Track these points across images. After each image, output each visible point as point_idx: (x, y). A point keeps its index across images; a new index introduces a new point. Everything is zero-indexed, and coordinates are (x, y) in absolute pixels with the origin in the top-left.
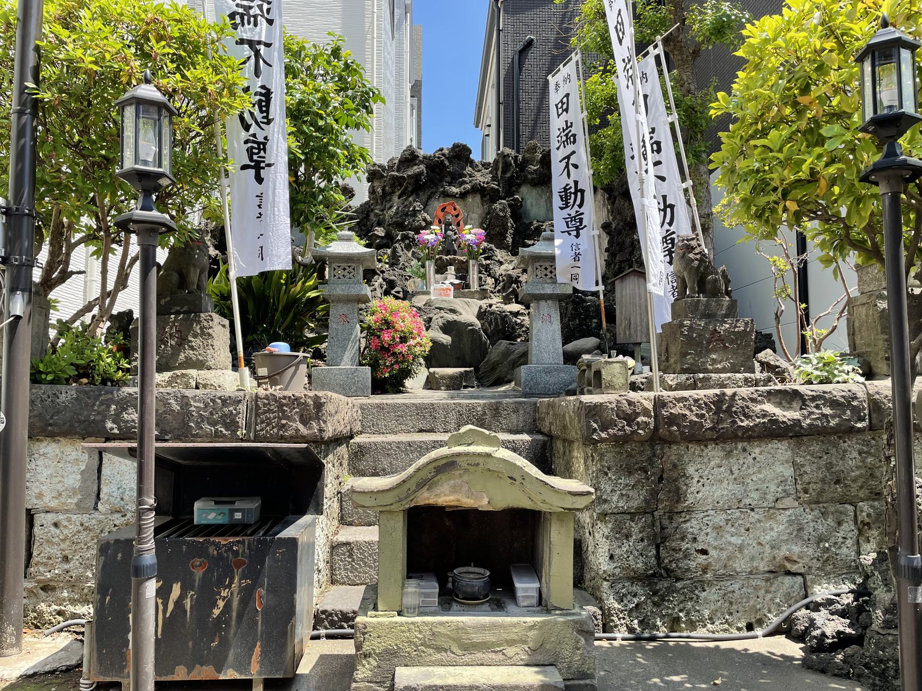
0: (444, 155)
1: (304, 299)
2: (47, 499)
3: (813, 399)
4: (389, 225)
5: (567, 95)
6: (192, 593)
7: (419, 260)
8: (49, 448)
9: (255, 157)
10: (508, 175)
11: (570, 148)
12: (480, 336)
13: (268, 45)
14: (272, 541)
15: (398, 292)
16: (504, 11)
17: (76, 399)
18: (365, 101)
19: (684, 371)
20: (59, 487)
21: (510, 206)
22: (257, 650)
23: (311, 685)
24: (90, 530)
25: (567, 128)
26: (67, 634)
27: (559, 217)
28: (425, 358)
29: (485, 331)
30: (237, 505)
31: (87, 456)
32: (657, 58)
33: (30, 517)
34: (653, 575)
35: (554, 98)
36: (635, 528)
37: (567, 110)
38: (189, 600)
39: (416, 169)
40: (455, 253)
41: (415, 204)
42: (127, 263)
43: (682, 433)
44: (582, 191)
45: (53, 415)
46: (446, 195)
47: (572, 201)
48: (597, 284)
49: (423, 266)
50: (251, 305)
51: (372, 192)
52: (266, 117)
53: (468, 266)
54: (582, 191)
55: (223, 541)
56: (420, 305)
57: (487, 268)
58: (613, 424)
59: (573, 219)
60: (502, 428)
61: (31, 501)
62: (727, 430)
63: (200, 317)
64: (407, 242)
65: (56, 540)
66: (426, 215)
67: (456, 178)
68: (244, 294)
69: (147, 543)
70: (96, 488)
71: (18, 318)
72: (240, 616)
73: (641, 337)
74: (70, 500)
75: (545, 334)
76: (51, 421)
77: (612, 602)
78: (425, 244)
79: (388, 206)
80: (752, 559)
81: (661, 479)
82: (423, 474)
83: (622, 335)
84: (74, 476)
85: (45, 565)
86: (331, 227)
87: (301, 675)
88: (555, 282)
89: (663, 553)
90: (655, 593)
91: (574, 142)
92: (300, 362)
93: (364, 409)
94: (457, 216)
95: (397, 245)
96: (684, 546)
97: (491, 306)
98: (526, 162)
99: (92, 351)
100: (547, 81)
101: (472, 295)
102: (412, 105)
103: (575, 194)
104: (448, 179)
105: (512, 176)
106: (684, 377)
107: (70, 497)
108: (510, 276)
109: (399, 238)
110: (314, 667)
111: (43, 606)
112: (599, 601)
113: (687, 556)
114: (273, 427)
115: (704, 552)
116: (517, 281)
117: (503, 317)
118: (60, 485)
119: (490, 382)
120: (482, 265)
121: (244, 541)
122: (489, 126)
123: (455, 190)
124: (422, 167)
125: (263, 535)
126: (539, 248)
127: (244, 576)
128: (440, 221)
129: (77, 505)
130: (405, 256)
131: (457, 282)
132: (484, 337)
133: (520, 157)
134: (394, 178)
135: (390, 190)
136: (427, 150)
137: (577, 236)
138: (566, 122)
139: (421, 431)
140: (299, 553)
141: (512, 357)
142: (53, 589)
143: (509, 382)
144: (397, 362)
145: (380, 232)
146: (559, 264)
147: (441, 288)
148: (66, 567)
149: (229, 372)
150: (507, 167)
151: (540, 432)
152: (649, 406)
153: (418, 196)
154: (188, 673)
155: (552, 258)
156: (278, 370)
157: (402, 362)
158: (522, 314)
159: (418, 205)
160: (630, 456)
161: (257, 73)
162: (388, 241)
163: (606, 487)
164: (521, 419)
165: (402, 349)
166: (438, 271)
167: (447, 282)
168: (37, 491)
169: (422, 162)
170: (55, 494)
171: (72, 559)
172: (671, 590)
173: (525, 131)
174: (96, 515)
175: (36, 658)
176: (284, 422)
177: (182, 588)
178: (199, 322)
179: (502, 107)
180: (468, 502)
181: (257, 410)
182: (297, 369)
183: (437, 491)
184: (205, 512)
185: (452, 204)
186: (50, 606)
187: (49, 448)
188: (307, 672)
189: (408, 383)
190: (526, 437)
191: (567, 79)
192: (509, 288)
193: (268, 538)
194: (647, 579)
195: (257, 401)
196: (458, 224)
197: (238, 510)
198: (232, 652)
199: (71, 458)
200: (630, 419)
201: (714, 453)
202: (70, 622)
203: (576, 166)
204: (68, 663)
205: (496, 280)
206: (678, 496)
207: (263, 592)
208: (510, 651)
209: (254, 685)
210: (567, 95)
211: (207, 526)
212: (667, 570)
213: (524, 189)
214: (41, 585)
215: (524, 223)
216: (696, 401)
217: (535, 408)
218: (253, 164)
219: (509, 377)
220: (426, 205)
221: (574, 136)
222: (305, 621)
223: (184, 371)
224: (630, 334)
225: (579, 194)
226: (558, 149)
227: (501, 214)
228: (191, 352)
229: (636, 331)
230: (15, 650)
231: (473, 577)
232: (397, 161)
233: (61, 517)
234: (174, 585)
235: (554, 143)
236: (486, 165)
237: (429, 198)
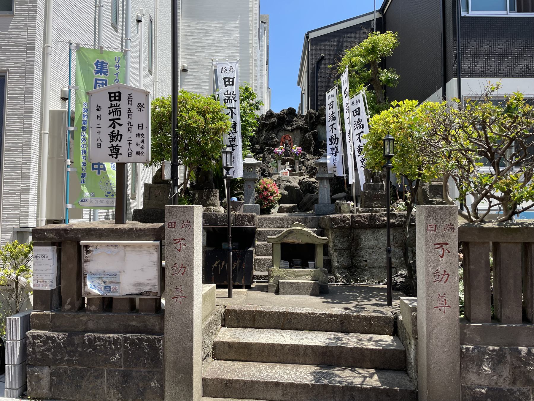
0: (284, 113)
3: (399, 216)
5: (333, 102)
10: (312, 121)
11: (333, 122)
12: (300, 192)
13: (235, 108)
19: (365, 207)
22: (244, 278)
28: (278, 201)
32: (363, 95)
34: (350, 267)
35: (328, 102)
36: (345, 254)
37: (332, 107)
43: (359, 226)
44: (338, 138)
48: (343, 174)
49: (276, 162)
52: (235, 131)
56: (275, 179)
58: (339, 223)
59: (334, 149)
62: (372, 225)
67: (289, 123)
72: (239, 269)
75: (324, 192)
77: (338, 275)
80: (380, 263)
81: (353, 239)
82: (285, 234)
89: (353, 261)
90: (351, 272)
96: (360, 259)
97: (304, 179)
100: (325, 95)
101: (296, 175)
103: (335, 139)
106: (364, 209)
108: (312, 167)
112: (334, 275)
113: (360, 262)
115: (366, 261)
117: (309, 184)
120: (300, 161)
123: (289, 128)
124: (275, 119)
126: (322, 160)
130: (268, 157)
131: (290, 169)
132: (302, 192)
133: (317, 113)
136: (277, 111)
137: (336, 156)
139: (279, 227)
143: (311, 210)
144: (269, 203)
145: (258, 147)
147: (284, 172)
151: (320, 228)
152: (349, 218)
155: (326, 164)
160: (344, 232)
162: (261, 151)
163: (337, 241)
166: (282, 164)
169: (275, 117)
172: (355, 272)
179: (310, 87)
180: (296, 241)
183: (289, 238)
189: (272, 210)
190: (316, 229)
191: (333, 95)
192: (312, 172)
194: (348, 268)
196: (291, 144)
200: (344, 221)
201: (369, 232)
203: (335, 129)
206: (358, 244)
208: (307, 277)
210: (333, 102)
212: (355, 266)
213: (319, 127)
216: (364, 216)
217: (319, 219)
221: (335, 117)
231: (298, 261)
236: (302, 116)
237: (278, 131)
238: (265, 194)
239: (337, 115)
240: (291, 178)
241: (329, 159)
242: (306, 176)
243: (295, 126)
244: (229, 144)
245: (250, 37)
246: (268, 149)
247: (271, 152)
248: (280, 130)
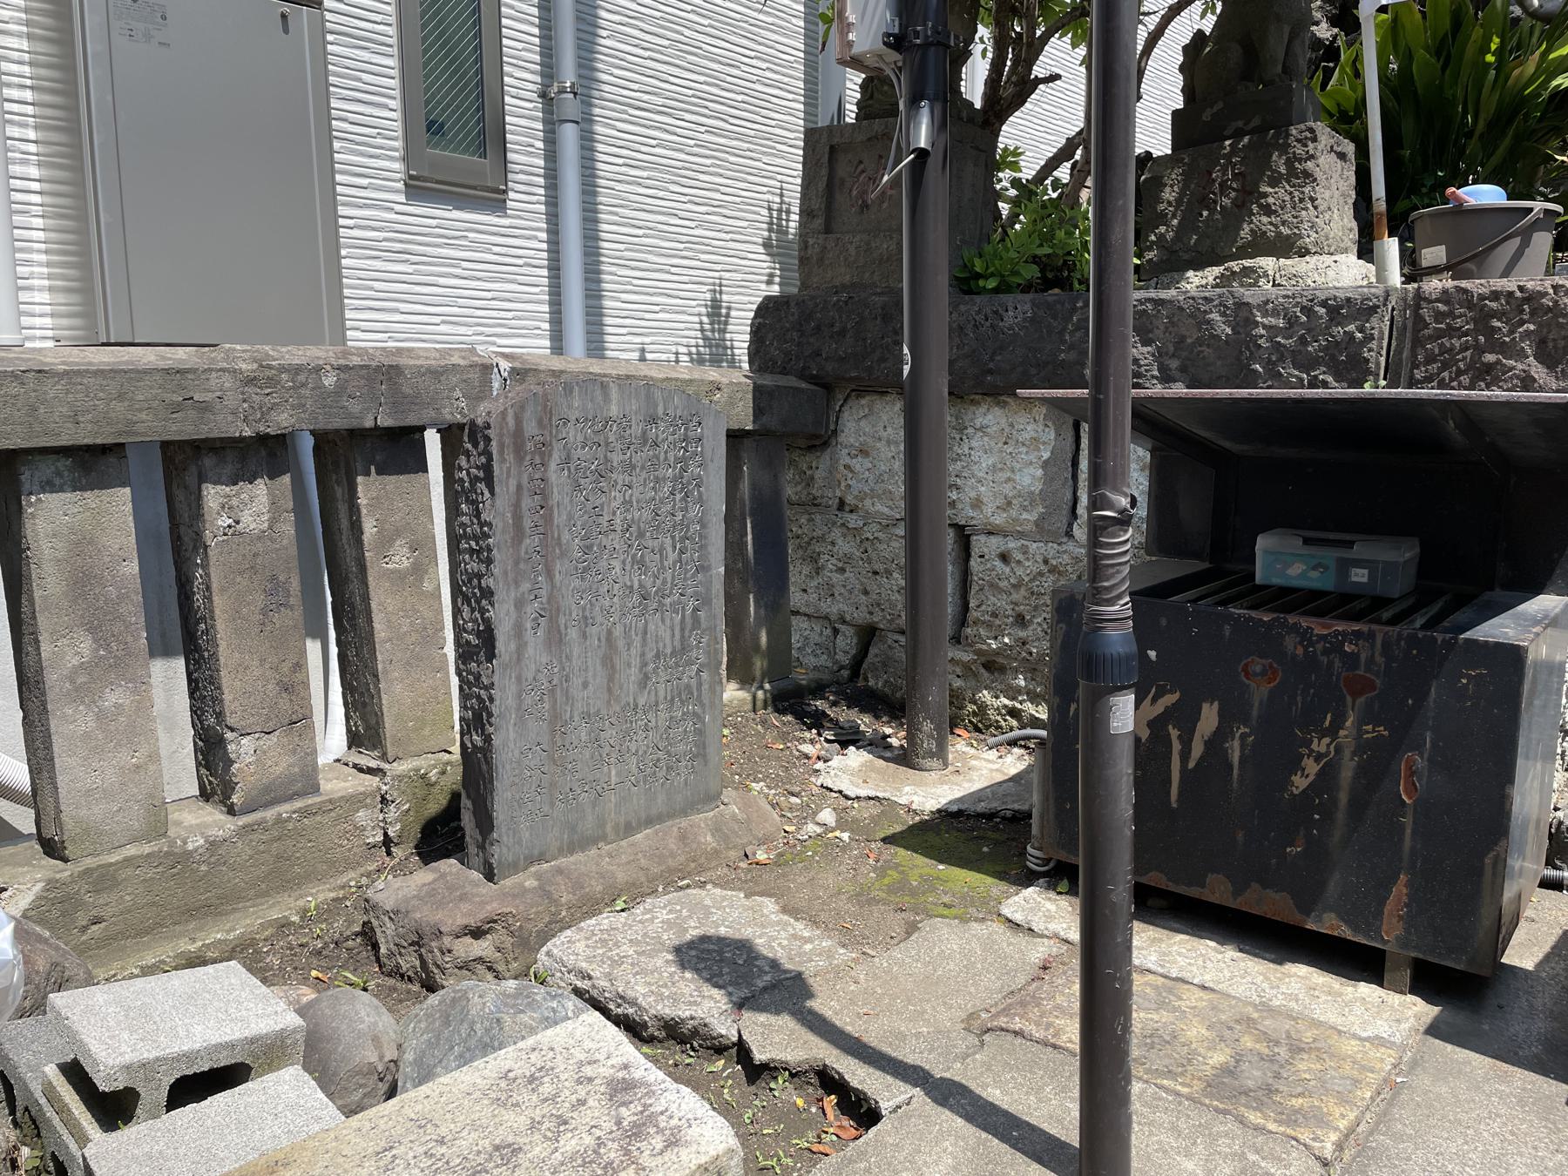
1: (1545, 95)
2: (989, 509)
6: (1243, 730)
8: (989, 417)
14: (1450, 645)
17: (1032, 320)
20: (1007, 489)
22: (1400, 890)
23: (1538, 1003)
24: (1060, 573)
26: (1022, 751)
30: (1359, 551)
31: (1053, 436)
33: (964, 537)
38: (1236, 744)
42: (1140, 48)
45: (994, 353)
50: (1408, 127)
55: (1317, 626)
61: (966, 514)
63: (1288, 135)
65: (1004, 584)
68: (1393, 104)
69: (1111, 602)
70: (1069, 496)
71: (922, 154)
72: (1358, 806)
74: (1025, 516)
76: (991, 365)
84: (1031, 470)
85: (989, 625)
87: (1512, 969)
92: (1536, 226)
99: (1070, 234)
107: (1025, 509)
110: (1547, 958)
111: (986, 696)
114: (1460, 373)
118: (1009, 486)
121: (1371, 636)
125: (1423, 627)
127: (1368, 716)
129: (1037, 524)
140: (1526, 687)
142: (1002, 669)
148: (1022, 634)
149: (1352, 258)
154: (1237, 893)
156: (1476, 240)
168: (973, 494)
170: (1000, 501)
171: (1031, 621)
174: (1070, 546)
175: (966, 785)
176: (1490, 358)
177: (1221, 714)
178: (1284, 148)
181: (1416, 331)
182: (1526, 243)
184: (1279, 558)
186: (997, 697)
187: (990, 417)
188: (1528, 964)
193: (1439, 637)
195: (1418, 307)
197: (1359, 563)
198: (1337, 876)
199: (1026, 435)
202: (1029, 731)
204: (1016, 807)
207: (1420, 762)
209: (1388, 964)
211: (1284, 591)
214: (983, 659)
222: (1530, 848)
223: (1247, 263)
228: (1265, 219)
230: (935, 763)
233: (1012, 544)
234: (1205, 706)
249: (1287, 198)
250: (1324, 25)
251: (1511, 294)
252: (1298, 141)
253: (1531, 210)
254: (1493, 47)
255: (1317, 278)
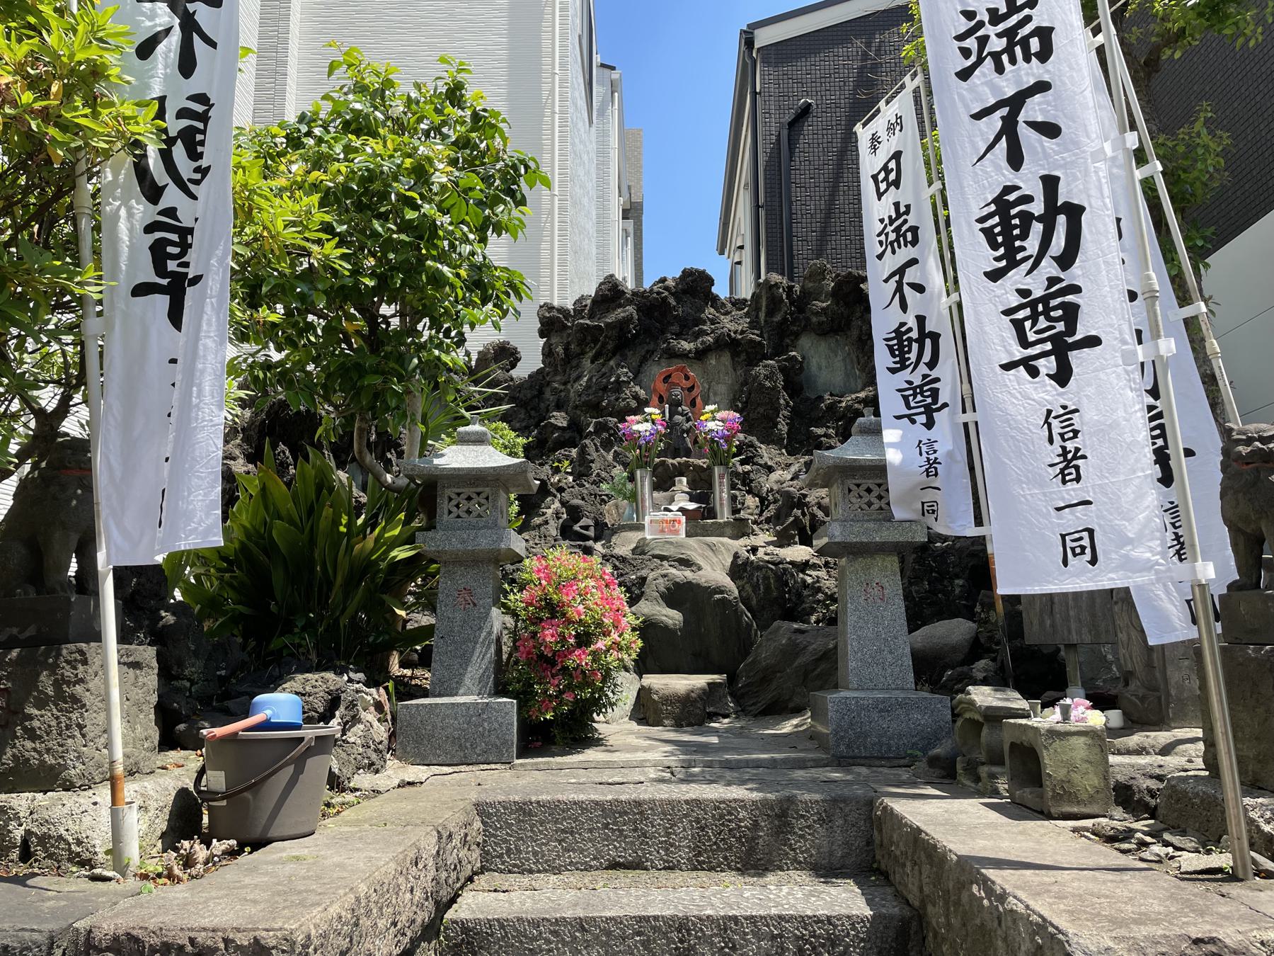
0: (667, 288)
1: (383, 565)
4: (576, 407)
5: (897, 156)
7: (625, 465)
9: (172, 266)
10: (778, 318)
11: (905, 254)
12: (738, 615)
15: (586, 528)
16: (763, 62)
18: (510, 183)
21: (782, 370)
25: (899, 215)
27: (889, 387)
29: (746, 601)
35: (870, 163)
37: (896, 183)
39: (620, 313)
40: (688, 453)
41: (620, 371)
44: (935, 337)
46: (673, 355)
47: (913, 356)
49: (632, 478)
51: (548, 353)
53: (711, 476)
54: (935, 337)
57: (746, 479)
59: (917, 390)
60: (795, 860)
63: (59, 654)
64: (605, 435)
66: (637, 388)
73: (1079, 633)
75: (874, 628)
78: (633, 438)
79: (574, 375)
83: (1036, 627)
86: (463, 417)
88: (890, 518)
91: (915, 242)
93: (489, 815)
94: (691, 389)
95: (587, 441)
97: (754, 550)
98: (807, 296)
101: (719, 531)
102: (625, 230)
103: (921, 342)
104: (675, 328)
105: (785, 320)
108: (787, 495)
109: (591, 429)
116: (801, 503)
117: (781, 574)
119: (760, 707)
120: (735, 474)
122: (741, 247)
123: (686, 345)
124: (631, 309)
126: (853, 451)
128: (661, 399)
130: (600, 458)
131: (692, 506)
133: (797, 288)
134: (584, 329)
135: (578, 350)
137: (929, 425)
138: (897, 205)
141: (801, 660)
143: (797, 711)
144: (569, 687)
146: (895, 485)
147: (663, 519)
150: (774, 303)
153: (624, 358)
155: (879, 470)
157: (581, 687)
158: (815, 567)
159: (624, 373)
161: (187, 64)
164: (839, 837)
165: (582, 659)
166: (656, 487)
167: (674, 507)
169: (630, 302)
173: (802, 249)
178: (53, 669)
179: (762, 212)
182: (299, 770)
185: (682, 370)
192: (793, 519)
196: (693, 404)
203: (919, 288)
205: (762, 500)
210: (897, 156)
213: (806, 342)
215: (808, 399)
218: (165, 282)
219: (797, 700)
220: (637, 373)
221: (914, 230)
224: (1053, 625)
225: (928, 342)
226: (880, 257)
227: (768, 384)
228: (29, 744)
229: (1067, 619)
232: (589, 302)
235: (872, 246)
236: (738, 304)
238: (549, 635)
239: (921, 217)
240: (695, 548)
241: (896, 445)
242: (762, 538)
243: (710, 339)
244: (148, 275)
245: (546, 43)
246: (601, 428)
247: (610, 438)
248: (651, 353)
249: (54, 723)
250: (241, 461)
251: (182, 947)
252: (68, 662)
253: (302, 739)
254: (344, 522)
255: (71, 826)
